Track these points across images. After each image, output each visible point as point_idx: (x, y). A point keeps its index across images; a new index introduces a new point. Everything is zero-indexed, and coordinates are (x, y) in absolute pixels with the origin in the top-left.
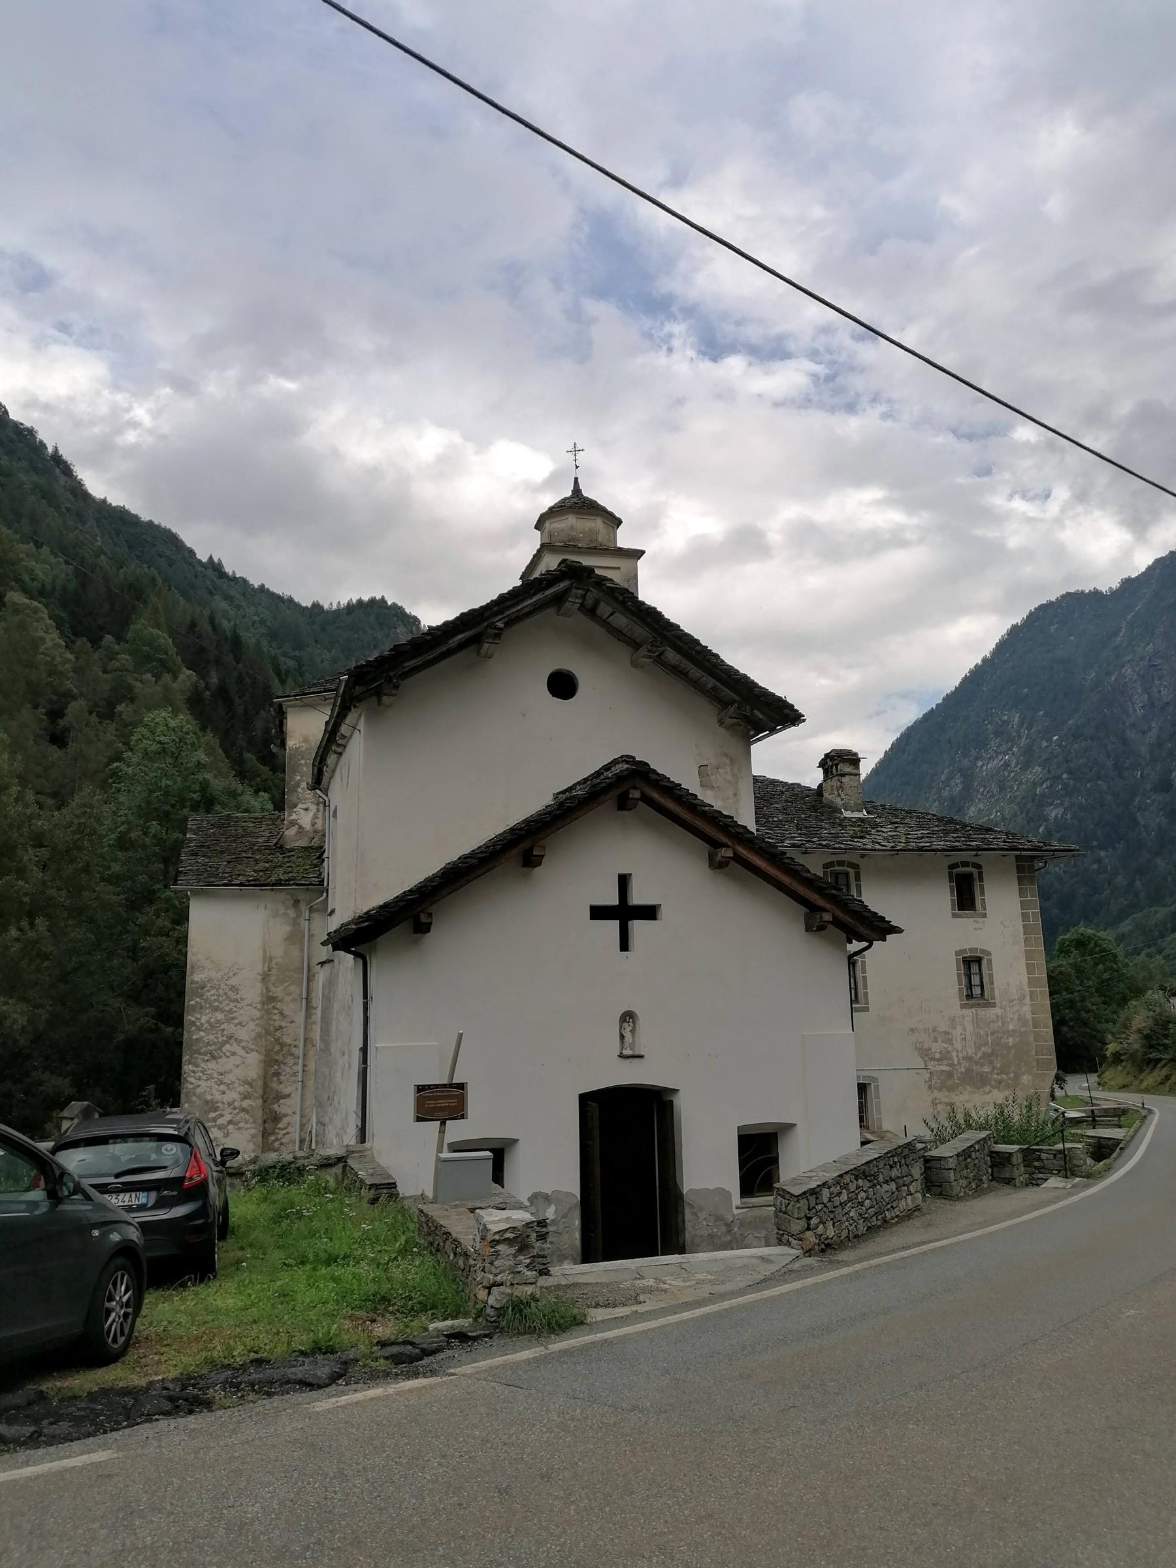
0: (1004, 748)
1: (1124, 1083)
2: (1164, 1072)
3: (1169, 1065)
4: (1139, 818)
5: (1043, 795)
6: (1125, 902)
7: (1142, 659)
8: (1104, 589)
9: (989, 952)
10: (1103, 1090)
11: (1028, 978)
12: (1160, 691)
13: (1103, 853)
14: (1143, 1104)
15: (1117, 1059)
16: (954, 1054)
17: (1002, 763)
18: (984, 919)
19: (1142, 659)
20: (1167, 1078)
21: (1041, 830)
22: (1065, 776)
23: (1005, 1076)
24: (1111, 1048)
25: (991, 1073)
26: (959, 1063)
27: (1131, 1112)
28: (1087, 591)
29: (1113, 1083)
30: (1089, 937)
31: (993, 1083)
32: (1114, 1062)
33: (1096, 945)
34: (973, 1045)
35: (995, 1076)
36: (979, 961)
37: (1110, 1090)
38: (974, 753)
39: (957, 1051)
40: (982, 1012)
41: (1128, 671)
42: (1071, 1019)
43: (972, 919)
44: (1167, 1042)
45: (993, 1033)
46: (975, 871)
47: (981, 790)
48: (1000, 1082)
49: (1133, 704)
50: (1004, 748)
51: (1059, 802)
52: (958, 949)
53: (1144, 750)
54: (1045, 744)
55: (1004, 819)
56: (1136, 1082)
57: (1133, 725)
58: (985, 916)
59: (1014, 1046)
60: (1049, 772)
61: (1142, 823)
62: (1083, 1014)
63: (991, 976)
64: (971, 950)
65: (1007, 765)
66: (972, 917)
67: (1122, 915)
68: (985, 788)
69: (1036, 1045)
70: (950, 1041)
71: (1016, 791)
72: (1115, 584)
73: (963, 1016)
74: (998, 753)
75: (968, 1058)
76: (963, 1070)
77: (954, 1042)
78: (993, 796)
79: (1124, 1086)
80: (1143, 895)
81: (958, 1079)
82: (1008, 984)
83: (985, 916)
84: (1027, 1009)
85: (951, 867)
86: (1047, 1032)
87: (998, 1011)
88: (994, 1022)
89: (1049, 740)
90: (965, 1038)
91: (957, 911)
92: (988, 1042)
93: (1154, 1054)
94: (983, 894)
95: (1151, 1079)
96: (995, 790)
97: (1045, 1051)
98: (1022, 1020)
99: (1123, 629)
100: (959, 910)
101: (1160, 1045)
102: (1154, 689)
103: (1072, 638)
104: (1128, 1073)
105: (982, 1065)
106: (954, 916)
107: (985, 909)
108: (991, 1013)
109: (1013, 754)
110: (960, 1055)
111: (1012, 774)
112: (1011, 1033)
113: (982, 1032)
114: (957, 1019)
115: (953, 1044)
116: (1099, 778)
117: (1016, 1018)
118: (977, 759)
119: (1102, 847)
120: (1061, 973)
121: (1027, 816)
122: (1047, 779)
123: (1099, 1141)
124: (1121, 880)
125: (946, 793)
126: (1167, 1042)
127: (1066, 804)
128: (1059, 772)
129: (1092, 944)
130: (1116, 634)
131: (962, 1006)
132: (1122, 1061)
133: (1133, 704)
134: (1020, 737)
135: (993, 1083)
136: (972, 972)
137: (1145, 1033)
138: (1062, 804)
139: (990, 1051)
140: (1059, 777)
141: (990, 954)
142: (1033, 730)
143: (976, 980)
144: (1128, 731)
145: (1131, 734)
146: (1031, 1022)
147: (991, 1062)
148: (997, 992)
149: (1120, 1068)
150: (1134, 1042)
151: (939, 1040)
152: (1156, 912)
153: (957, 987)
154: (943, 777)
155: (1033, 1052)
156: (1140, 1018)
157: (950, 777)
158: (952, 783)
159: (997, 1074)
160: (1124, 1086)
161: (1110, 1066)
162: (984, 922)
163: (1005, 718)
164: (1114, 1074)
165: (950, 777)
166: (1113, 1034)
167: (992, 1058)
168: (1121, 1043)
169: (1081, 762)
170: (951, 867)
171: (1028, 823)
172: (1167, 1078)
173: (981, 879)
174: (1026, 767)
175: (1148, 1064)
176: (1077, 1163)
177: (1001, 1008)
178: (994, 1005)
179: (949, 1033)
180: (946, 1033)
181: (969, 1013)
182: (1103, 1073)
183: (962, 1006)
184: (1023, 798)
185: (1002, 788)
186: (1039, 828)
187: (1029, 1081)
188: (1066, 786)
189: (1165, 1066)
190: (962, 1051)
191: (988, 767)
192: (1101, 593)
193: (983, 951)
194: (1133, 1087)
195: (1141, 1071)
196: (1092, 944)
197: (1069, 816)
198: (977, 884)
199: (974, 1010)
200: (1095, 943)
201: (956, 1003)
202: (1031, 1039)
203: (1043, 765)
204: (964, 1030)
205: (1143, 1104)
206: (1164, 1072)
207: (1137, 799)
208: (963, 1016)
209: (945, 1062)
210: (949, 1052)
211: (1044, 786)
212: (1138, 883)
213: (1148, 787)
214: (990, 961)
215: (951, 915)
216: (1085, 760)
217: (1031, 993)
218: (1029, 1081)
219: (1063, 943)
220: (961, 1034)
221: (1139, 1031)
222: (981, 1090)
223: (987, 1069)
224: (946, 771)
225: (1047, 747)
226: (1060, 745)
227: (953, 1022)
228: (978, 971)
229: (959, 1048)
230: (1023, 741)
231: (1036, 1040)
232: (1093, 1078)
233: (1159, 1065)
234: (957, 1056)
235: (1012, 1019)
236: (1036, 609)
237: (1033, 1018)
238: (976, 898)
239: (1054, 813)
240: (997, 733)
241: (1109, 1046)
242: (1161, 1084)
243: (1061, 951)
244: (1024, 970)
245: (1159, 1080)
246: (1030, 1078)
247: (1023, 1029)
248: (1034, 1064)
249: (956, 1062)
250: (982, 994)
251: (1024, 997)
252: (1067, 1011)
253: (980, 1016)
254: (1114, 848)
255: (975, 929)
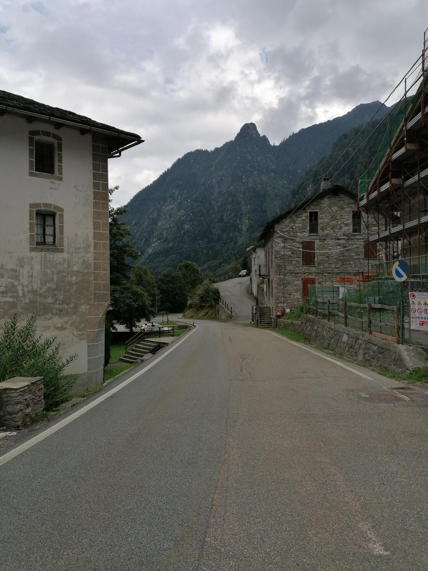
0: (172, 202)
1: (192, 315)
2: (206, 311)
3: (208, 308)
4: (213, 231)
5: (184, 220)
6: (206, 259)
7: (219, 176)
8: (209, 150)
9: (61, 208)
10: (184, 318)
11: (94, 232)
12: (223, 188)
13: (200, 242)
14: (193, 324)
15: (191, 306)
16: (20, 288)
17: (171, 207)
18: (59, 182)
19: (219, 176)
20: (207, 313)
21: (182, 232)
22: (191, 214)
23: (66, 306)
24: (189, 302)
25: (54, 303)
26: (24, 295)
27: (189, 327)
28: (204, 150)
29: (188, 316)
30: (190, 264)
31: (54, 311)
32: (189, 308)
33: (192, 267)
34: (39, 281)
35: (57, 306)
36: (53, 215)
37: (186, 318)
38: (162, 203)
39: (23, 286)
40: (50, 256)
41: (214, 180)
42: (180, 293)
43: (49, 180)
44: (208, 299)
45: (58, 273)
46: (55, 141)
47: (163, 216)
48: (61, 311)
49: (214, 192)
50: (172, 202)
51: (188, 223)
52: (33, 202)
53: (216, 208)
54: (186, 202)
55: (170, 227)
56: (196, 315)
57: (214, 199)
58: (61, 179)
59: (77, 283)
60: (186, 212)
61: (213, 232)
62: (184, 292)
63: (62, 228)
64: (45, 205)
65: (173, 208)
66: (49, 178)
67: (204, 262)
68: (165, 216)
69: (95, 283)
70: (17, 278)
71: (175, 218)
72: (213, 149)
73: (32, 258)
74: (170, 204)
75: (33, 292)
76: (27, 301)
77: (21, 278)
78: (167, 219)
79: (192, 317)
80: (211, 256)
81: (22, 308)
82: (76, 235)
83: (61, 179)
84: (90, 257)
85: (33, 133)
86: (105, 274)
87: (65, 255)
88: (60, 264)
89: (187, 201)
90: (32, 276)
91: (34, 171)
92: (53, 279)
93: (203, 304)
94: (60, 161)
95: (201, 314)
96: (168, 217)
97: (102, 288)
98: (85, 263)
99: (214, 166)
100: (36, 171)
101: (206, 301)
102: (221, 188)
103: (197, 166)
104: (194, 312)
105: (46, 297)
106: (31, 174)
107: (61, 174)
108: (58, 257)
109: (175, 205)
110: (26, 289)
111: (174, 212)
112: (74, 273)
113: (48, 272)
114: (26, 260)
115: (19, 280)
116: (202, 216)
117: (80, 261)
118: (163, 205)
119: (200, 240)
120: (178, 276)
121: (178, 227)
122: (185, 215)
123: (159, 344)
124: (205, 251)
125: (151, 217)
126: (208, 299)
127: (191, 224)
128: (189, 213)
129: (190, 267)
130: (211, 167)
131: (32, 250)
132: (192, 307)
133: (214, 192)
134: (178, 199)
135: (54, 311)
136: (47, 223)
137: (201, 296)
138: (189, 224)
139: (54, 286)
140: (189, 215)
141: (62, 210)
142: (182, 197)
143: (49, 231)
144: (212, 201)
145: (213, 202)
146: (92, 265)
147: (55, 295)
148: (65, 242)
149: (191, 310)
150: (197, 299)
151: (5, 276)
152: (215, 262)
153: (28, 234)
154: (151, 211)
155: (92, 288)
156: (200, 290)
157: (153, 211)
158: (154, 213)
159: (59, 304)
160: (192, 317)
161: (188, 309)
162: (59, 184)
163: (174, 192)
164: (189, 313)
165: (153, 211)
166: (190, 297)
167: (56, 292)
168: (193, 300)
169: (196, 210)
170: (33, 133)
171: (178, 230)
172: (207, 313)
173: (60, 148)
174: (179, 210)
175: (201, 308)
176: (10, 409)
177: (68, 253)
178: (62, 251)
179: (16, 271)
180: (13, 270)
181: (37, 256)
182: (186, 312)
183: (32, 250)
184: (177, 221)
185: (170, 217)
186: (181, 231)
187: (87, 309)
188: (191, 217)
189: (206, 309)
190: (27, 286)
191: (166, 209)
192: (208, 151)
193: (56, 207)
194: (195, 317)
195: (198, 311)
196: (190, 267)
197: (191, 228)
198: (56, 152)
199: (43, 254)
200: (192, 266)
201: (27, 246)
202: (92, 278)
203: (184, 210)
204: (32, 269)
205: (193, 324)
206: (206, 311)
207: (213, 224)
208: (32, 258)
209: (9, 294)
210: (14, 286)
211: (184, 217)
212: (210, 252)
213: (216, 220)
214: (62, 216)
215: (28, 174)
216: (198, 209)
217: (95, 244)
218: (87, 309)
219: (181, 265)
220: (28, 272)
221: (199, 295)
222: (42, 317)
223: (50, 300)
224: (152, 208)
225: (186, 204)
226: (190, 203)
227: (21, 262)
228: (52, 224)
229: (26, 283)
230: (179, 201)
231: (95, 279)
232: (182, 314)
233: (205, 308)
234: (23, 290)
235: (77, 263)
236: (187, 154)
237: (94, 263)
238: (55, 165)
239: (186, 227)
240: (170, 197)
241: (189, 301)
242: (204, 315)
243: (179, 269)
244: (91, 226)
245: (204, 314)
246: (88, 307)
247: (85, 271)
248: (92, 297)
249: (21, 294)
250: (54, 242)
251: (89, 246)
252: (178, 290)
253: (48, 259)
254: (204, 240)
255: (51, 188)
